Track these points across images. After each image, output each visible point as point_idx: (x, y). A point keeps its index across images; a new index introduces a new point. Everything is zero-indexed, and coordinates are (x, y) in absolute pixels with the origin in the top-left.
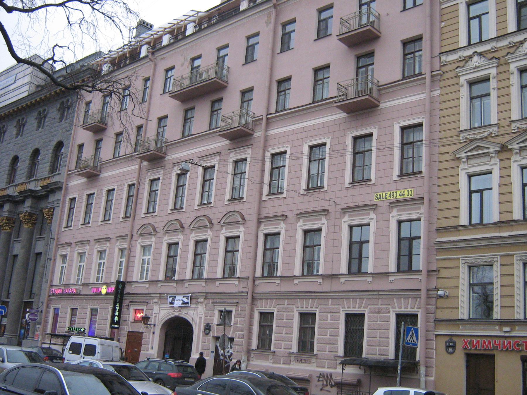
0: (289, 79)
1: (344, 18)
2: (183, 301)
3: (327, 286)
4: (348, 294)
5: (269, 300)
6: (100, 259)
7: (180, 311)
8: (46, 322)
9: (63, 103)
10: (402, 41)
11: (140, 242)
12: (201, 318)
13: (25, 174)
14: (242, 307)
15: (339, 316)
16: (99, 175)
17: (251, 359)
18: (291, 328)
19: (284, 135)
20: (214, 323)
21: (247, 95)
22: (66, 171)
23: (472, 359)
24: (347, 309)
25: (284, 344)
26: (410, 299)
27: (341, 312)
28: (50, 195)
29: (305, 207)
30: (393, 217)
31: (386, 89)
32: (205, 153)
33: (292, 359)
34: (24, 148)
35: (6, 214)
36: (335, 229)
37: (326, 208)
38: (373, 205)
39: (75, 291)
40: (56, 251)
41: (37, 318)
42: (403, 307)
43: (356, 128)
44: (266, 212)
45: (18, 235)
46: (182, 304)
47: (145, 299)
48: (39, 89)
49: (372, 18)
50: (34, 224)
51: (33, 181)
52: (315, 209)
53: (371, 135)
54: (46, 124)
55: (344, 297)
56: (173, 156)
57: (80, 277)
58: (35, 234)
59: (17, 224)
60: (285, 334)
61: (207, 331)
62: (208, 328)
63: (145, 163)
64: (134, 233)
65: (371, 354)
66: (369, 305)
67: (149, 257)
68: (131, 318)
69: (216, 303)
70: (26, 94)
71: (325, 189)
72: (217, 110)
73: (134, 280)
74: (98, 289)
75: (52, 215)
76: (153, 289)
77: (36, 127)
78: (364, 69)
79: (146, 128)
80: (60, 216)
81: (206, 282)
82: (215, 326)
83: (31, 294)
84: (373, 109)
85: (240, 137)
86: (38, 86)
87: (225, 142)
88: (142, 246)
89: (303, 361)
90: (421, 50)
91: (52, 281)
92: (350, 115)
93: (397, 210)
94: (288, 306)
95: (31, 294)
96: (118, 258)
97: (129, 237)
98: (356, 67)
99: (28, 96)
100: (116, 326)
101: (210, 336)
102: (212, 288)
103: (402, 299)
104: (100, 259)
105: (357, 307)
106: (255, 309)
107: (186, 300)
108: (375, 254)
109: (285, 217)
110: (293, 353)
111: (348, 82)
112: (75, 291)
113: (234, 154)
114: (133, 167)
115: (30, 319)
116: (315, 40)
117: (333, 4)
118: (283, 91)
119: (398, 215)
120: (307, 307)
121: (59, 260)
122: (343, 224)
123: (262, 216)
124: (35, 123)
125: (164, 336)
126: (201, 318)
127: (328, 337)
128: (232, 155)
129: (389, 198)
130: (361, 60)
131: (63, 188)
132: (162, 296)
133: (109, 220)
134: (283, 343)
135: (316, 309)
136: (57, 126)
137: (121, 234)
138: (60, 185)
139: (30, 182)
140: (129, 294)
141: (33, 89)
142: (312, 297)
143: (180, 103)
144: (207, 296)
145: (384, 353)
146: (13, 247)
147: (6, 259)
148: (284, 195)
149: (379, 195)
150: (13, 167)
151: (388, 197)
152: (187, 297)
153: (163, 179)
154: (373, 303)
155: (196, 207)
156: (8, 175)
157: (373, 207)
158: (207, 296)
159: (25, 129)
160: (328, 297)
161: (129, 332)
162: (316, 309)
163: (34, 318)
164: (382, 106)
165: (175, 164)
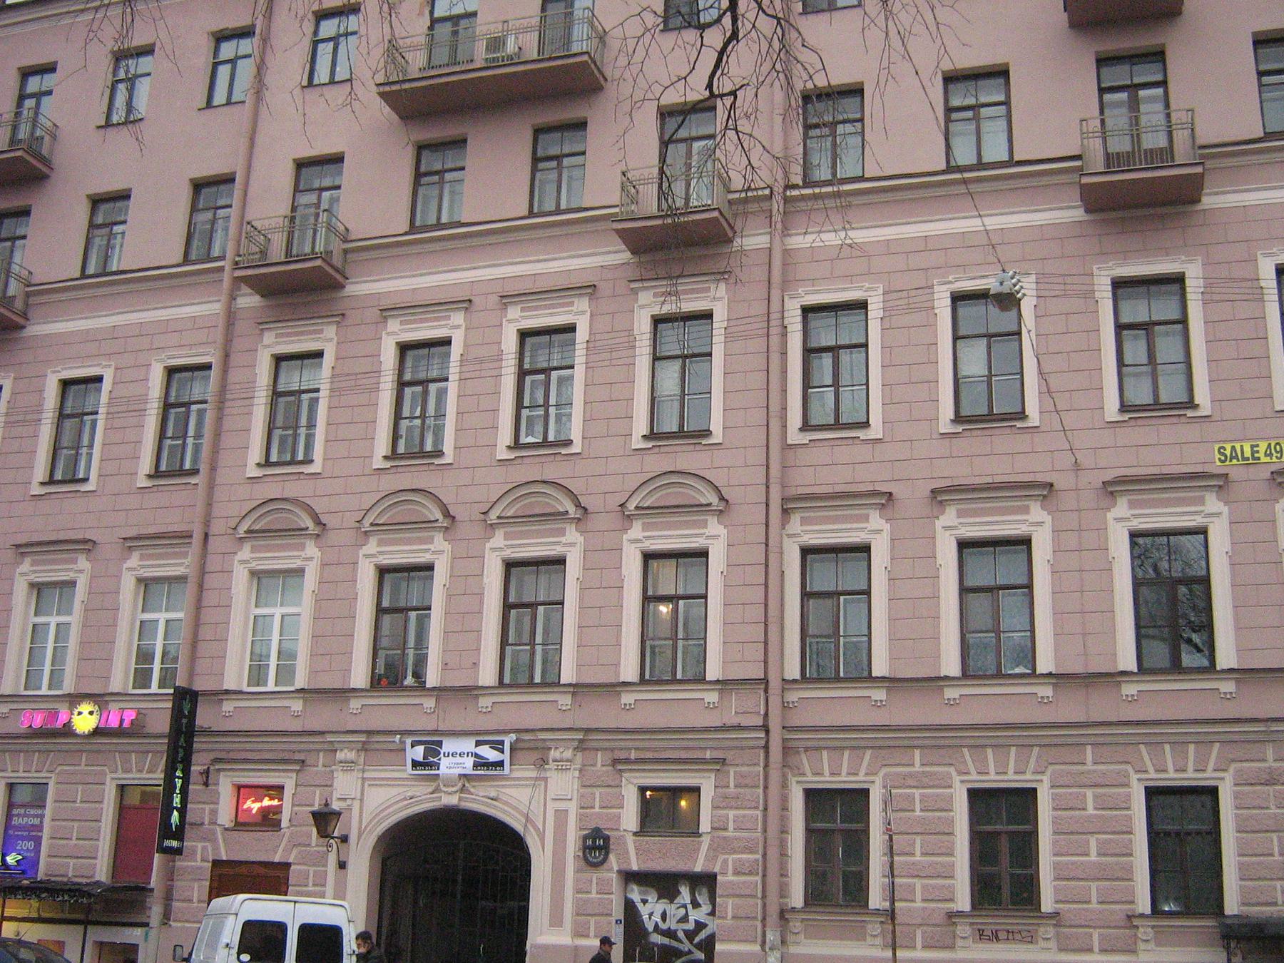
2: (477, 755)
3: (1071, 708)
4: (1154, 731)
7: (463, 789)
11: (245, 560)
12: (561, 815)
14: (740, 775)
15: (1129, 795)
16: (23, 327)
17: (790, 938)
18: (945, 838)
19: (87, 337)
20: (624, 826)
23: (856, 890)
25: (923, 886)
26: (846, 753)
29: (962, 473)
30: (494, 549)
32: (528, 286)
33: (963, 929)
36: (603, 562)
37: (1047, 478)
38: (86, 541)
43: (1125, 255)
44: (804, 481)
46: (476, 766)
47: (295, 750)
49: (38, 133)
52: (998, 479)
55: (1137, 739)
56: (1222, 198)
60: (923, 854)
61: (596, 856)
62: (596, 846)
63: (249, 301)
64: (218, 527)
65: (1068, 902)
66: (1233, 761)
68: (225, 816)
69: (627, 761)
71: (448, 459)
73: (229, 685)
74: (54, 715)
76: (323, 717)
78: (8, 244)
79: (246, 185)
81: (574, 694)
82: (630, 839)
84: (1180, 209)
85: (676, 243)
87: (619, 255)
89: (1002, 935)
92: (636, 260)
94: (1095, 767)
96: (26, 617)
100: (175, 844)
101: (610, 870)
102: (602, 714)
105: (1190, 767)
106: (793, 780)
107: (490, 754)
108: (580, 635)
109: (87, 545)
110: (960, 914)
113: (277, 336)
116: (99, 127)
117: (56, 63)
119: (35, 572)
120: (1002, 772)
123: (793, 492)
125: (379, 872)
126: (561, 815)
128: (269, 338)
129: (1267, 459)
132: (373, 744)
133: (86, 480)
134: (918, 883)
135: (1038, 777)
137: (151, 530)
140: (208, 732)
142: (1020, 741)
143: (395, 117)
144: (586, 740)
149: (1228, 447)
151: (1261, 455)
152: (498, 745)
154: (1247, 757)
155: (143, 482)
157: (87, 545)
158: (586, 740)
160: (1083, 740)
161: (217, 863)
162: (1038, 777)
164: (37, 329)
165: (387, 312)
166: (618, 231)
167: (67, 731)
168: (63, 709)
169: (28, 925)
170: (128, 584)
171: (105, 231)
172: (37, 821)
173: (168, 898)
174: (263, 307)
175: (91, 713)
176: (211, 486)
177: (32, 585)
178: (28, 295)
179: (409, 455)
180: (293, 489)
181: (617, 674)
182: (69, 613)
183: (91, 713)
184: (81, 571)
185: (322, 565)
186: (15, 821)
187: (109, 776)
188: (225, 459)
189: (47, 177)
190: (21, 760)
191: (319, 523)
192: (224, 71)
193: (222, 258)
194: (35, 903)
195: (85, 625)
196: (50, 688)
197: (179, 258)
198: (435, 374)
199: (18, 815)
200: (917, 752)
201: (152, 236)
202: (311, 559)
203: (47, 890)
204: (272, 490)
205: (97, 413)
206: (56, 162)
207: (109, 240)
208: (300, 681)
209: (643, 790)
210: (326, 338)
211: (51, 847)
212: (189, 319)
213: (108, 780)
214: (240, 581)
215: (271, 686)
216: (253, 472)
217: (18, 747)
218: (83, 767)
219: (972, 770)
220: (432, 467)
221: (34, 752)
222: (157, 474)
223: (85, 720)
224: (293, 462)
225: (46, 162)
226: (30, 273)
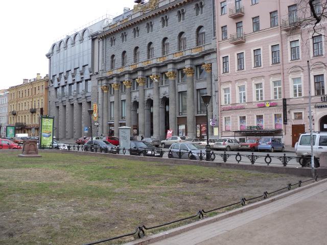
6: (240, 91)
9: (197, 5)
11: (291, 76)
22: (217, 41)
36: (250, 84)
50: (193, 73)
54: (128, 39)
63: (284, 33)
72: (240, 27)
95: (111, 118)
97: (282, 74)
114: (274, 35)
121: (223, 93)
131: (218, 52)
133: (261, 66)
147: (175, 94)
148: (262, 67)
153: (263, 49)
155: (236, 72)
159: (168, 22)
164: (247, 42)
170: (237, 88)
173: (285, 131)
176: (283, 64)
177: (292, 79)
179: (316, 56)
180: (297, 64)
182: (262, 88)
188: (284, 60)
191: (303, 69)
193: (277, 25)
195: (248, 92)
198: (319, 41)
201: (265, 22)
204: (294, 64)
210: (298, 37)
212: (274, 36)
214: (290, 80)
215: (298, 97)
216: (290, 62)
222: (273, 64)
225: (243, 13)
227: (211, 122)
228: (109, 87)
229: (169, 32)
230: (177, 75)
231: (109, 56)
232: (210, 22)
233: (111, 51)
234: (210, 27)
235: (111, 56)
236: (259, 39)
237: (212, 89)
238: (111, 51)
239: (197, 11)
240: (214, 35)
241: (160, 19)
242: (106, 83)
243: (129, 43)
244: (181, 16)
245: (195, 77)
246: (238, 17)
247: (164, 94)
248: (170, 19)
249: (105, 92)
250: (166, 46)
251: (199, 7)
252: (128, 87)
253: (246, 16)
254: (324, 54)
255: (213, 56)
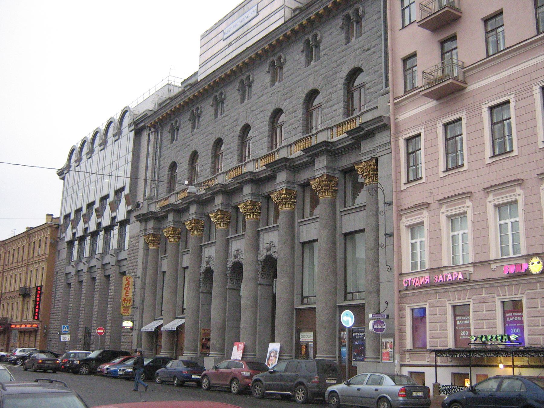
0: (500, 13)
1: (424, 3)
5: (506, 287)
8: (402, 331)
10: (482, 19)
13: (300, 128)
16: (465, 88)
21: (409, 62)
22: (391, 99)
24: (452, 302)
26: (514, 286)
27: (447, 305)
28: (362, 143)
31: (469, 71)
34: (289, 95)
35: (249, 198)
38: (518, 180)
39: (460, 276)
40: (399, 220)
41: (383, 327)
42: (507, 294)
45: (303, 215)
48: (297, 12)
50: (335, 191)
51: (153, 203)
53: (460, 119)
54: (322, 53)
57: (419, 260)
58: (296, 218)
59: (162, 242)
67: (422, 239)
70: (281, 22)
75: (377, 170)
77: (239, 100)
78: (449, 53)
80: (393, 169)
83: (346, 293)
86: (294, 10)
88: (449, 217)
90: (503, 25)
91: (400, 267)
92: (441, 101)
93: (493, 195)
95: (346, 293)
96: (448, 231)
98: (440, 53)
99: (284, 23)
103: (538, 284)
104: (412, 238)
111: (432, 69)
112: (460, 276)
115: (375, 330)
118: (410, 69)
121: (405, 235)
122: (488, 204)
124: (212, 110)
127: (541, 327)
130: (490, 23)
133: (511, 151)
135: (425, 303)
136: (345, 50)
138: (385, 121)
139: (171, 196)
141: (289, 15)
145: (435, 345)
146: (299, 233)
147: (293, 248)
148: (515, 153)
150: (216, 152)
156: (269, 136)
157: (468, 195)
162: (521, 296)
163: (380, 327)
164: (471, 87)
166: (424, 95)
167: (528, 273)
168: (523, 262)
169: (524, 369)
170: (443, 219)
171: (494, 33)
172: (468, 322)
174: (439, 104)
175: (539, 263)
177: (496, 206)
178: (464, 73)
181: (489, 256)
182: (517, 216)
183: (539, 263)
184: (519, 195)
185: (473, 208)
186: (458, 323)
187: (497, 298)
189: (460, 17)
190: (506, 289)
192: (407, 11)
194: (526, 359)
195: (526, 221)
196: (514, 254)
197: (535, 33)
199: (459, 320)
200: (538, 284)
202: (468, 207)
203: (534, 351)
205: (510, 118)
206: (462, 10)
207: (497, 37)
208: (427, 267)
209: (413, 310)
211: (529, 331)
213: (447, 304)
217: (504, 284)
218: (438, 300)
219: (501, 294)
220: (460, 173)
221: (512, 285)
223: (536, 267)
224: (506, 153)
226: (463, 62)
227: (372, 322)
228: (157, 239)
229: (284, 95)
230: (299, 200)
231: (166, 164)
232: (376, 56)
233: (171, 153)
234: (376, 68)
235: (168, 165)
236: (505, 74)
237: (377, 228)
238: (171, 153)
239: (307, 56)
240: (387, 85)
241: (188, 116)
242: (288, 182)
243: (195, 139)
244: (174, 133)
245: (182, 245)
246: (444, 24)
247: (268, 250)
248: (287, 63)
249: (151, 247)
250: (356, 94)
251: (353, 22)
252: (250, 219)
253: (466, 16)
254: (423, 173)
255: (381, 139)
